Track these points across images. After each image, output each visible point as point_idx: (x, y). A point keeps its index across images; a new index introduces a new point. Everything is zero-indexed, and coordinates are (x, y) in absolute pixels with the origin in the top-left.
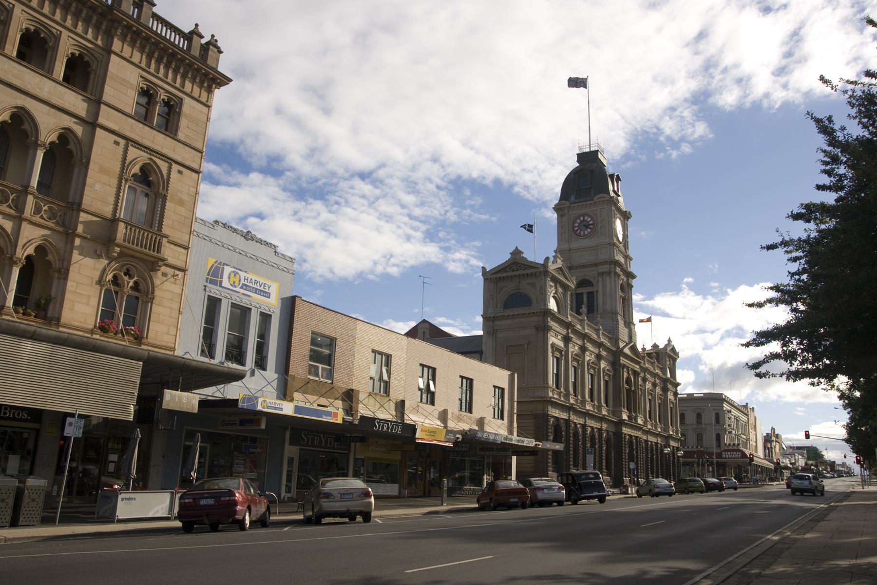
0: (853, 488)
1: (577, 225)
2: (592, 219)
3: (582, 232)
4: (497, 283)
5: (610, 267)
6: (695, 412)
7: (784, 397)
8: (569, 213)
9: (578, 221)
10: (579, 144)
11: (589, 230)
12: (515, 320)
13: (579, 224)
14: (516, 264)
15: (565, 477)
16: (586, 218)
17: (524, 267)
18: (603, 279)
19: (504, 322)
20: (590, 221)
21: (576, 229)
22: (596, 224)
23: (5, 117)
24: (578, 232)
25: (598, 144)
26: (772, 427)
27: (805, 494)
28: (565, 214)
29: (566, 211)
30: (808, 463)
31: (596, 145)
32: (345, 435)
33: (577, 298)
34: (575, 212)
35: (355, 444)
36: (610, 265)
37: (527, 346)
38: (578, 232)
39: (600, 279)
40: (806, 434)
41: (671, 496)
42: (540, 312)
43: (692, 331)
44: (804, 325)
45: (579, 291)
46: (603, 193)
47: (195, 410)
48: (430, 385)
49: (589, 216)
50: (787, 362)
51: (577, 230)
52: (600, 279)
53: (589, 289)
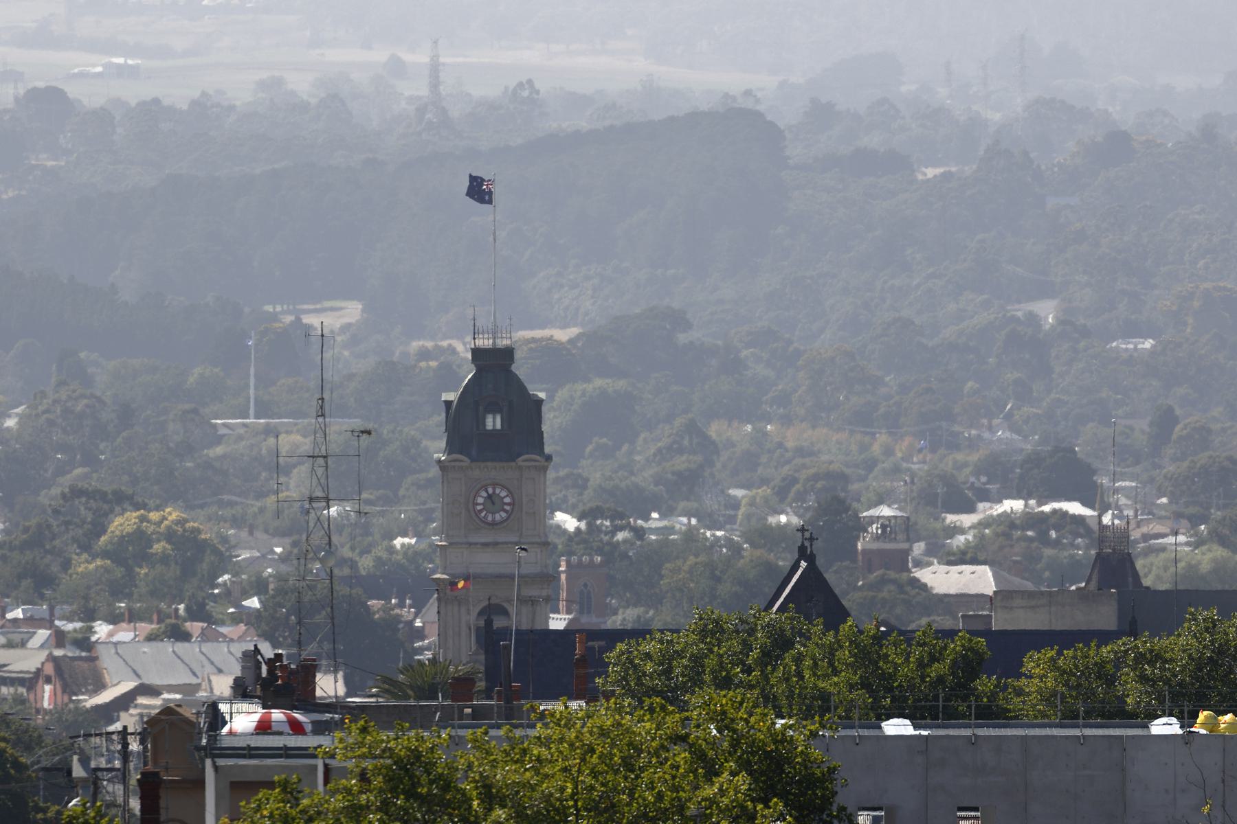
1: (480, 500)
2: (510, 494)
3: (484, 513)
7: (151, 638)
11: (498, 491)
13: (493, 513)
15: (315, 505)
16: (504, 515)
17: (357, 746)
20: (505, 497)
21: (479, 508)
22: (474, 515)
23: (2, 96)
24: (483, 514)
35: (494, 425)
38: (483, 514)
43: (236, 638)
44: (307, 598)
46: (523, 455)
47: (185, 107)
48: (207, 770)
49: (504, 487)
51: (481, 511)
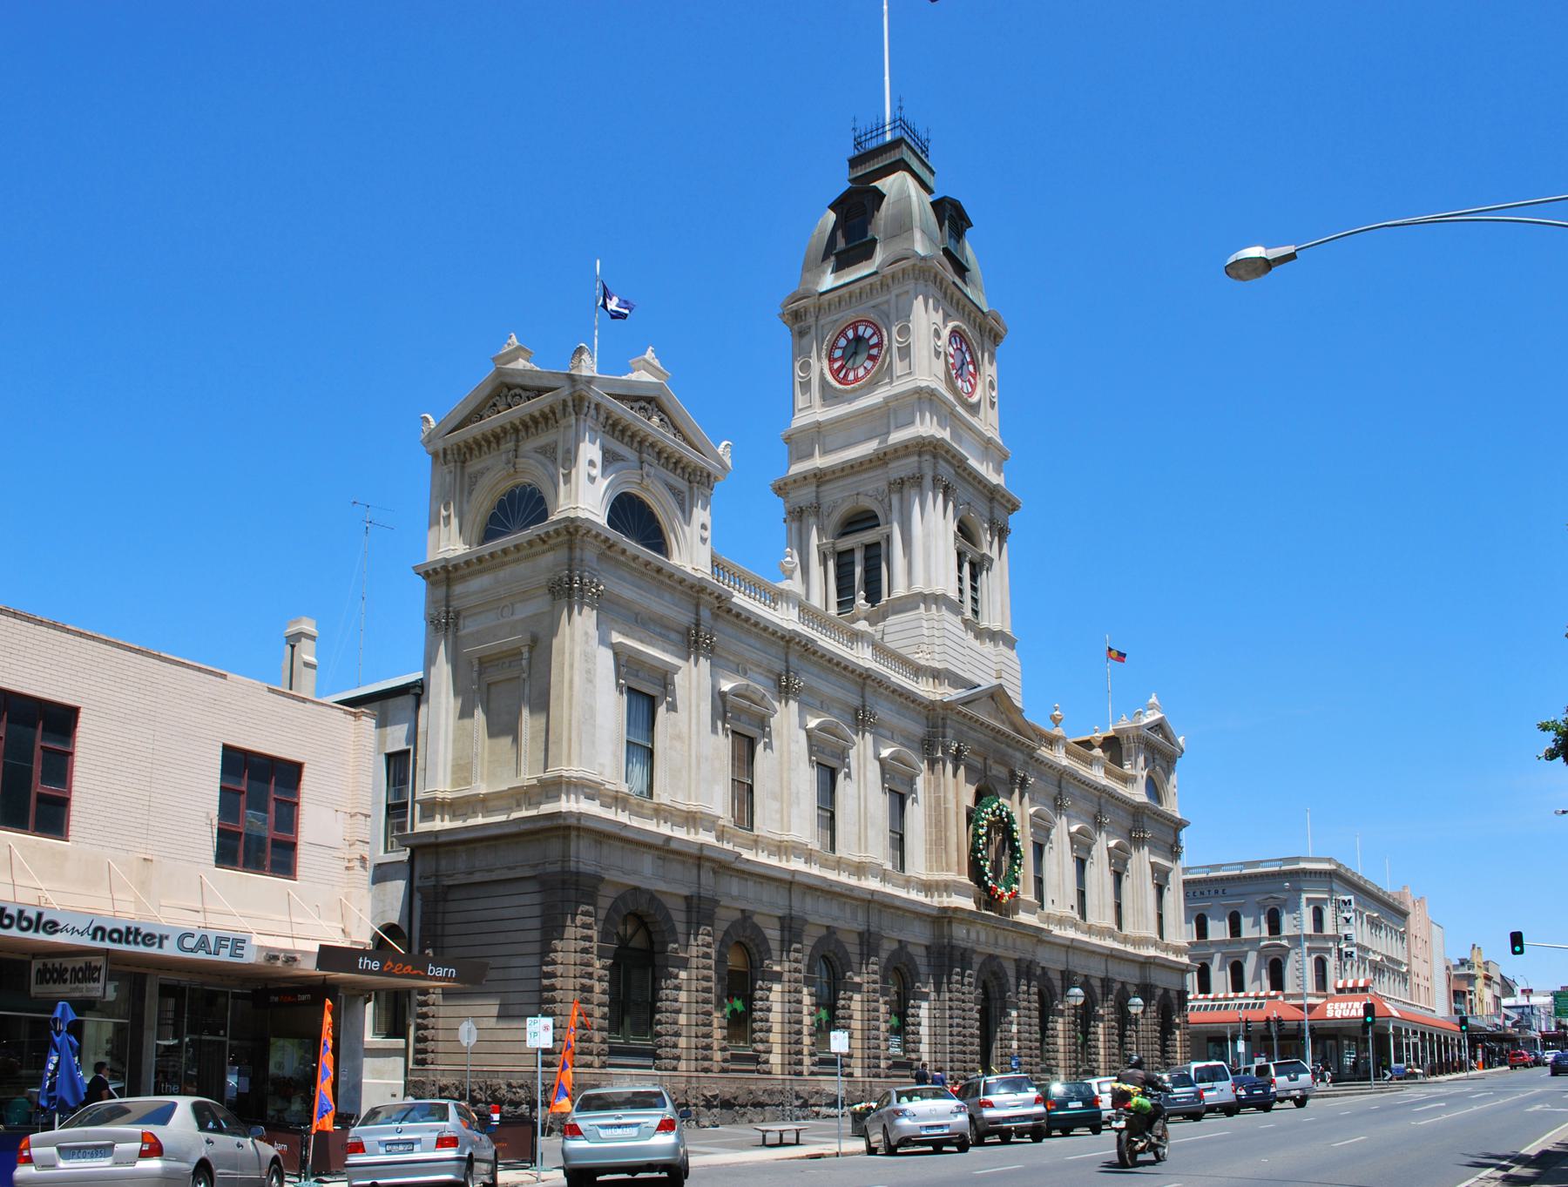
0: (239, 1145)
4: (464, 462)
5: (920, 462)
6: (1264, 907)
8: (822, 322)
9: (843, 342)
10: (854, 129)
12: (503, 574)
13: (844, 349)
14: (505, 390)
17: (524, 394)
18: (901, 500)
19: (475, 584)
25: (900, 119)
26: (1474, 945)
27: (945, 1149)
28: (809, 328)
29: (811, 320)
30: (1189, 976)
31: (898, 123)
32: (93, 965)
33: (838, 567)
34: (835, 317)
36: (920, 455)
37: (530, 652)
39: (895, 499)
40: (1521, 945)
41: (1232, 1115)
42: (557, 532)
45: (845, 544)
49: (869, 323)
50: (937, 312)
52: (895, 499)
53: (869, 537)
